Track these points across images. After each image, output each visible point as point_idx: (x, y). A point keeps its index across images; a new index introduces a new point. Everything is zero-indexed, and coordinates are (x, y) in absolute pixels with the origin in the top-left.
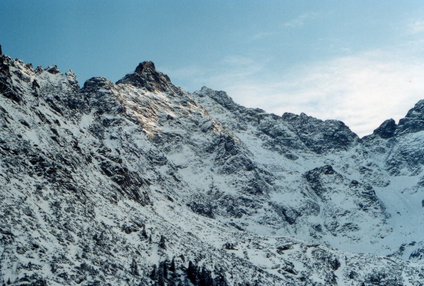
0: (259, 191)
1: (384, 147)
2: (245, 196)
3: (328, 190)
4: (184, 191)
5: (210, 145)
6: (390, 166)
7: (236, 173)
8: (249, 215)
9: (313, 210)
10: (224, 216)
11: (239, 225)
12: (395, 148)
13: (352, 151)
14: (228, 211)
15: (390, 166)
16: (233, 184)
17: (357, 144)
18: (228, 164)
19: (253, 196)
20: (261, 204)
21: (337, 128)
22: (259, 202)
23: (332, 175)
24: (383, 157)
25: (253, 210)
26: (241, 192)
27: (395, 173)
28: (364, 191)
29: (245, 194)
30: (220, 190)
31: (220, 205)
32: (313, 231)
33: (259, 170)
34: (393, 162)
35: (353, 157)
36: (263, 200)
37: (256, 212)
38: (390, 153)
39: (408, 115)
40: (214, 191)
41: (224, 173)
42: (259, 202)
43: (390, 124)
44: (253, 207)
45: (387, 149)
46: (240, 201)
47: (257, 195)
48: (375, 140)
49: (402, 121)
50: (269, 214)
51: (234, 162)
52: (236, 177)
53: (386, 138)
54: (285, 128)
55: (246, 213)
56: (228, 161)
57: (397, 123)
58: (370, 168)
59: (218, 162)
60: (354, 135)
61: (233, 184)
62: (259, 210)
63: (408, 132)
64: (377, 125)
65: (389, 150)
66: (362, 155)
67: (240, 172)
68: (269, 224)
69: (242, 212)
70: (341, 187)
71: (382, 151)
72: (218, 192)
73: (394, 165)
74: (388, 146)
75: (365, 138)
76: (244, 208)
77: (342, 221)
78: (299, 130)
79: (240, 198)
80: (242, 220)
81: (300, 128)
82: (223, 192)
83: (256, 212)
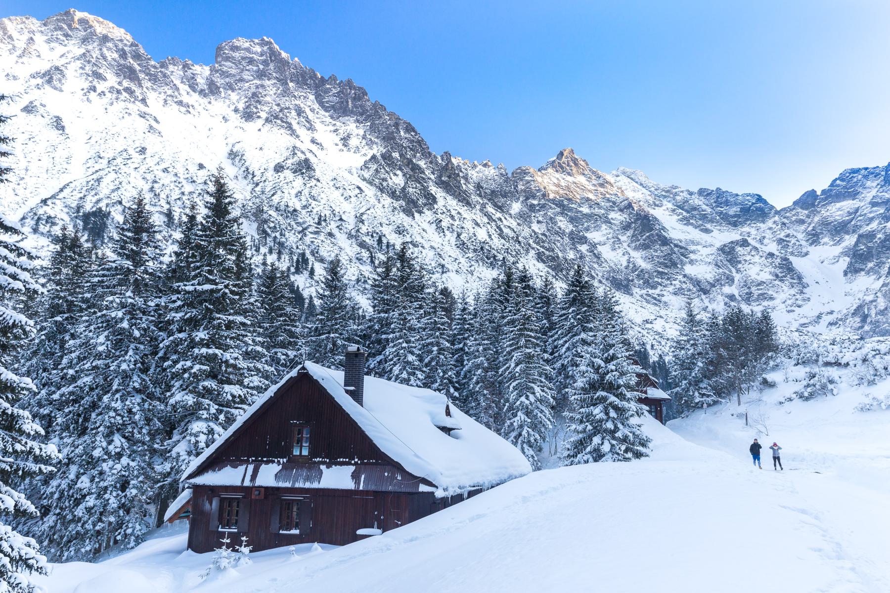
2: (660, 270)
38: (810, 224)
39: (832, 185)
44: (668, 279)
49: (824, 192)
53: (806, 209)
54: (701, 203)
58: (787, 239)
60: (772, 207)
62: (674, 282)
71: (802, 222)
76: (660, 280)
80: (657, 291)
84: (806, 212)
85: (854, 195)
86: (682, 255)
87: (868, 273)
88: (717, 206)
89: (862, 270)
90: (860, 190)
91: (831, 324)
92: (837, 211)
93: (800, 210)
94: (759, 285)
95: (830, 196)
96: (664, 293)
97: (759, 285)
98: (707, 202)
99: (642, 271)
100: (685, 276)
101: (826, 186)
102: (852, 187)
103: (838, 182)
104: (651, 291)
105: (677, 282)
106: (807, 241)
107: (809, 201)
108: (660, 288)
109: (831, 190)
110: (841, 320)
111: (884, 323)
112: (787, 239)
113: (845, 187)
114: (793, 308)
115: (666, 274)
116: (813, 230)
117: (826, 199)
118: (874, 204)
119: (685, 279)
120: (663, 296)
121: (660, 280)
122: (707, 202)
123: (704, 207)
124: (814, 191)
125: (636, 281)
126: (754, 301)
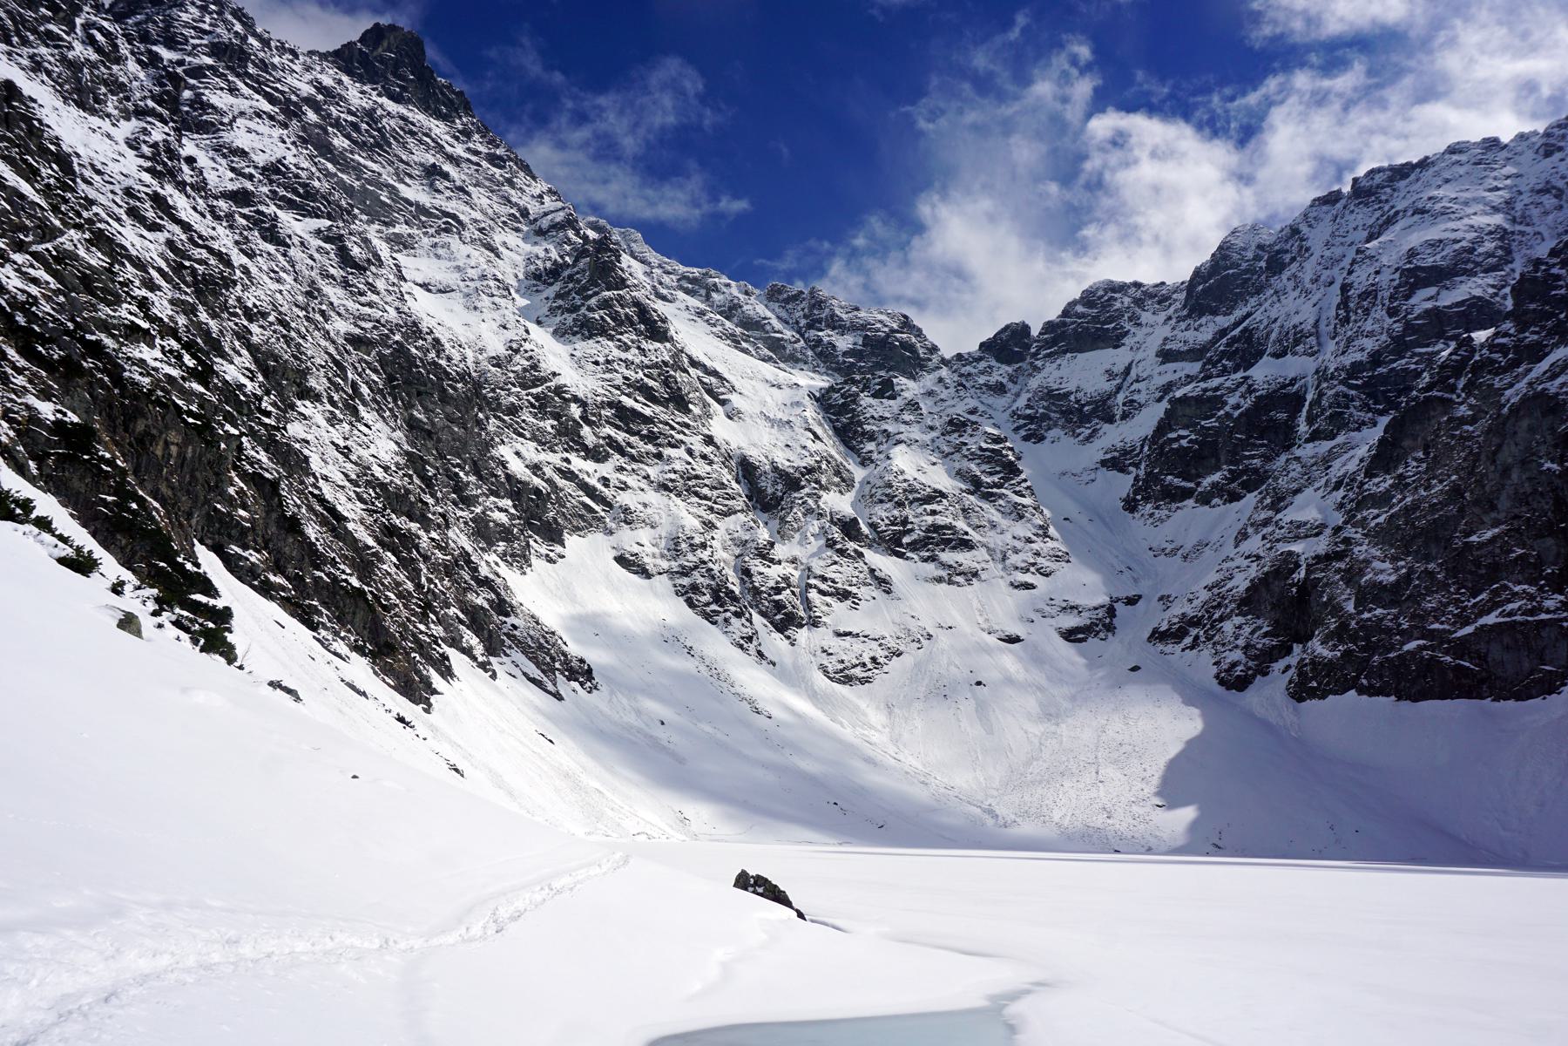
0: (679, 401)
1: (1004, 381)
2: (628, 402)
3: (881, 438)
4: (370, 305)
5: (548, 264)
6: (1022, 422)
7: (611, 338)
8: (633, 458)
9: (837, 479)
10: (541, 443)
11: (593, 482)
12: (1034, 383)
13: (928, 381)
14: (559, 433)
15: (1022, 422)
16: (597, 363)
17: (938, 368)
18: (590, 309)
19: (658, 409)
20: (681, 437)
21: (895, 326)
22: (673, 428)
23: (891, 402)
24: (1001, 402)
25: (650, 447)
26: (618, 388)
27: (1035, 437)
28: (984, 446)
29: (628, 395)
30: (542, 365)
31: (533, 406)
32: (836, 533)
33: (690, 357)
34: (1029, 412)
35: (930, 393)
36: (687, 426)
37: (659, 456)
38: (1018, 395)
39: (1065, 313)
40: (520, 362)
41: (574, 334)
42: (673, 428)
43: (1017, 333)
44: (651, 438)
45: (1010, 385)
46: (607, 412)
47: (671, 406)
48: (982, 365)
49: (1049, 327)
50: (701, 468)
51: (611, 307)
52: (609, 348)
53: (1009, 363)
54: (769, 314)
55: (622, 453)
56: (593, 301)
57: (1035, 332)
58: (973, 418)
59: (560, 302)
60: (934, 349)
61: (597, 363)
62: (668, 451)
63: (1065, 352)
64: (989, 333)
65: (1014, 388)
66: (952, 390)
67: (624, 338)
68: (697, 494)
69: (609, 445)
70: (915, 432)
71: (999, 389)
72: (535, 367)
73: (1031, 418)
74: (1013, 379)
75: (959, 357)
76: (621, 436)
77: (920, 519)
78: (803, 322)
79: (611, 405)
80: (606, 469)
81: (805, 317)
82: (554, 374)
83: (659, 456)
84: (1010, 369)
85: (1115, 340)
86: (710, 392)
87: (1205, 500)
88: (810, 326)
89: (1185, 494)
90: (1128, 326)
91: (1158, 636)
92: (1083, 374)
93: (994, 363)
94: (928, 500)
95: (1063, 337)
96: (631, 480)
97: (928, 500)
98: (784, 314)
99: (559, 390)
100: (709, 440)
101: (1053, 314)
102: (1111, 320)
103: (1080, 309)
104: (578, 463)
105: (680, 452)
106: (1017, 429)
107: (1010, 345)
108: (617, 459)
109: (1064, 324)
110: (1195, 622)
111: (1407, 636)
112: (973, 418)
113: (1095, 319)
114: (1028, 578)
115: (648, 420)
116: (1028, 407)
117: (1053, 342)
118: (1166, 356)
119: (708, 450)
120: (624, 487)
121: (621, 436)
122: (784, 314)
123: (777, 324)
124: (1024, 329)
125: (526, 415)
126: (914, 546)
